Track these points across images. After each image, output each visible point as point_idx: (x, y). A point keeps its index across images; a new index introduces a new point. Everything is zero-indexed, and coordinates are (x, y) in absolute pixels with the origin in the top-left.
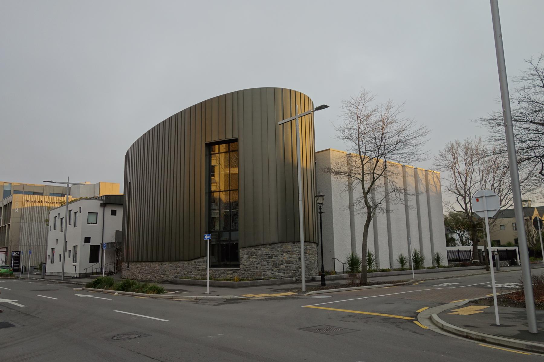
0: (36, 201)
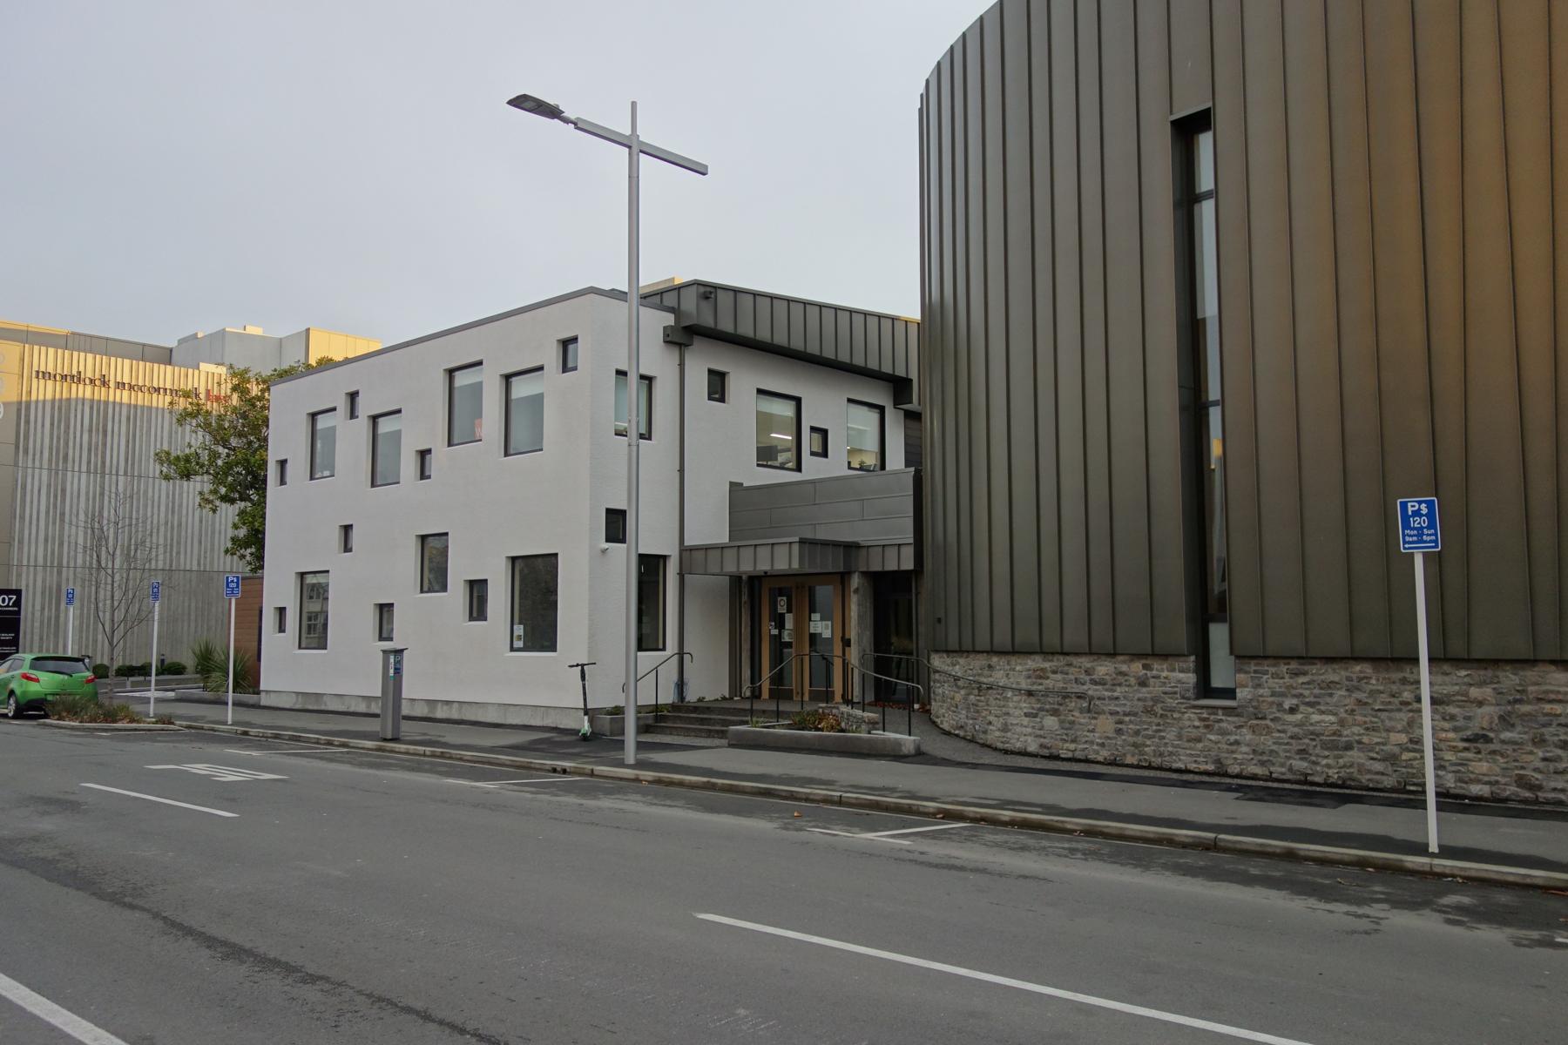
0: (78, 379)
